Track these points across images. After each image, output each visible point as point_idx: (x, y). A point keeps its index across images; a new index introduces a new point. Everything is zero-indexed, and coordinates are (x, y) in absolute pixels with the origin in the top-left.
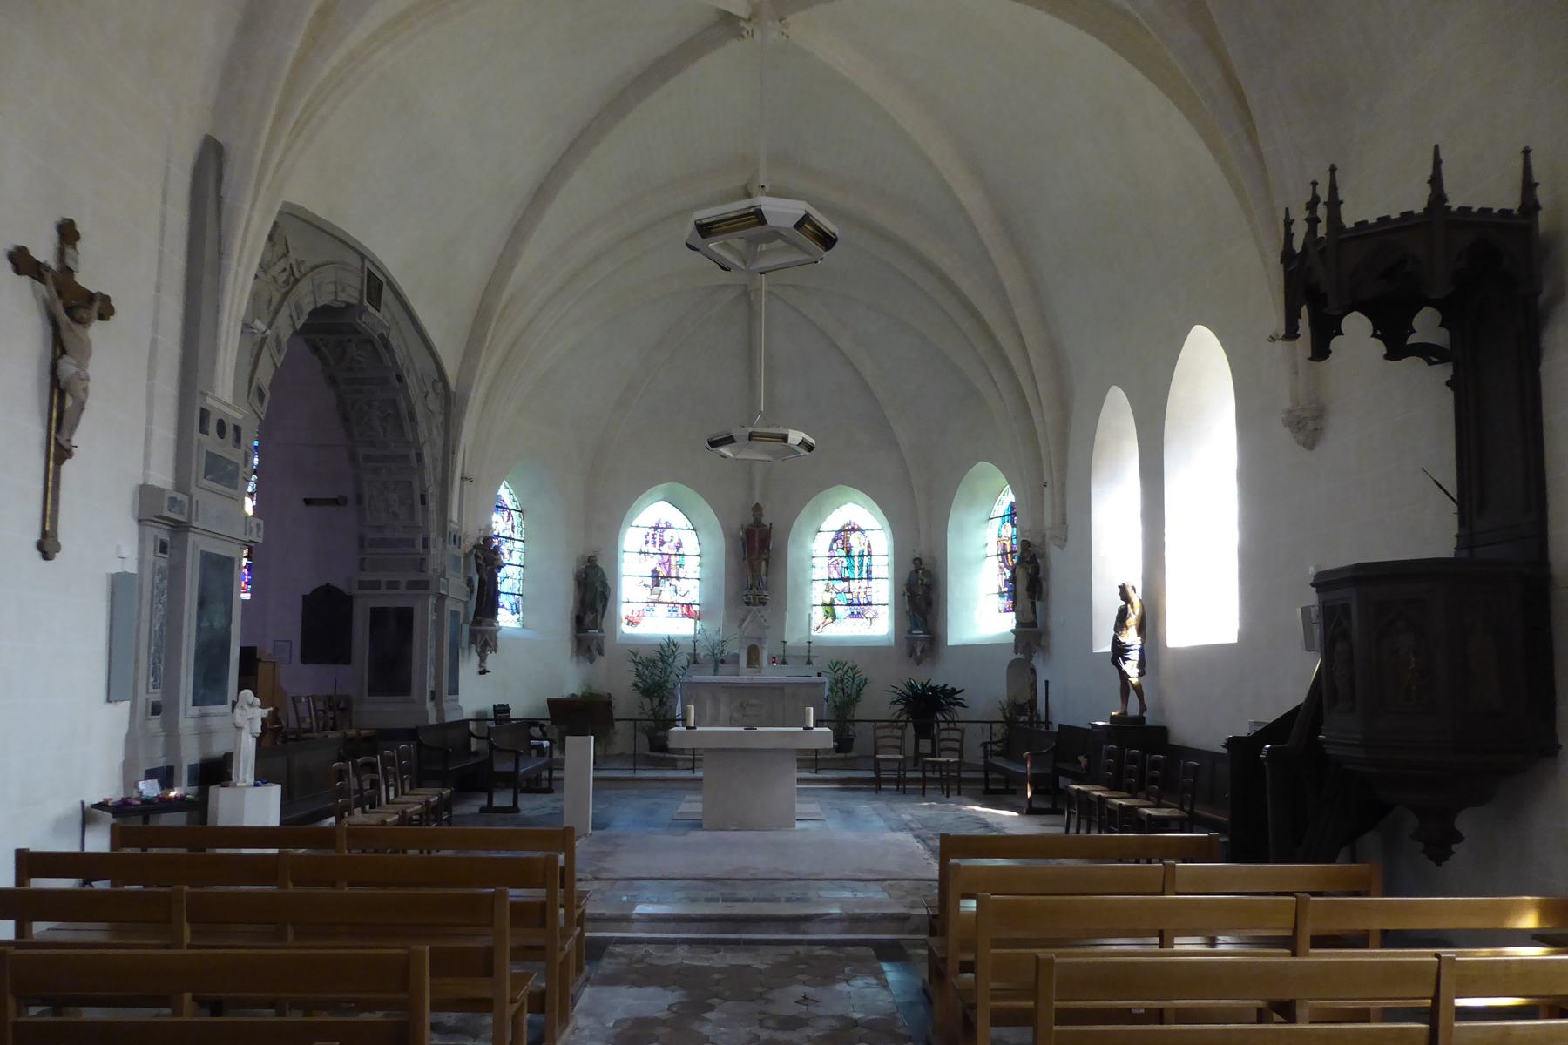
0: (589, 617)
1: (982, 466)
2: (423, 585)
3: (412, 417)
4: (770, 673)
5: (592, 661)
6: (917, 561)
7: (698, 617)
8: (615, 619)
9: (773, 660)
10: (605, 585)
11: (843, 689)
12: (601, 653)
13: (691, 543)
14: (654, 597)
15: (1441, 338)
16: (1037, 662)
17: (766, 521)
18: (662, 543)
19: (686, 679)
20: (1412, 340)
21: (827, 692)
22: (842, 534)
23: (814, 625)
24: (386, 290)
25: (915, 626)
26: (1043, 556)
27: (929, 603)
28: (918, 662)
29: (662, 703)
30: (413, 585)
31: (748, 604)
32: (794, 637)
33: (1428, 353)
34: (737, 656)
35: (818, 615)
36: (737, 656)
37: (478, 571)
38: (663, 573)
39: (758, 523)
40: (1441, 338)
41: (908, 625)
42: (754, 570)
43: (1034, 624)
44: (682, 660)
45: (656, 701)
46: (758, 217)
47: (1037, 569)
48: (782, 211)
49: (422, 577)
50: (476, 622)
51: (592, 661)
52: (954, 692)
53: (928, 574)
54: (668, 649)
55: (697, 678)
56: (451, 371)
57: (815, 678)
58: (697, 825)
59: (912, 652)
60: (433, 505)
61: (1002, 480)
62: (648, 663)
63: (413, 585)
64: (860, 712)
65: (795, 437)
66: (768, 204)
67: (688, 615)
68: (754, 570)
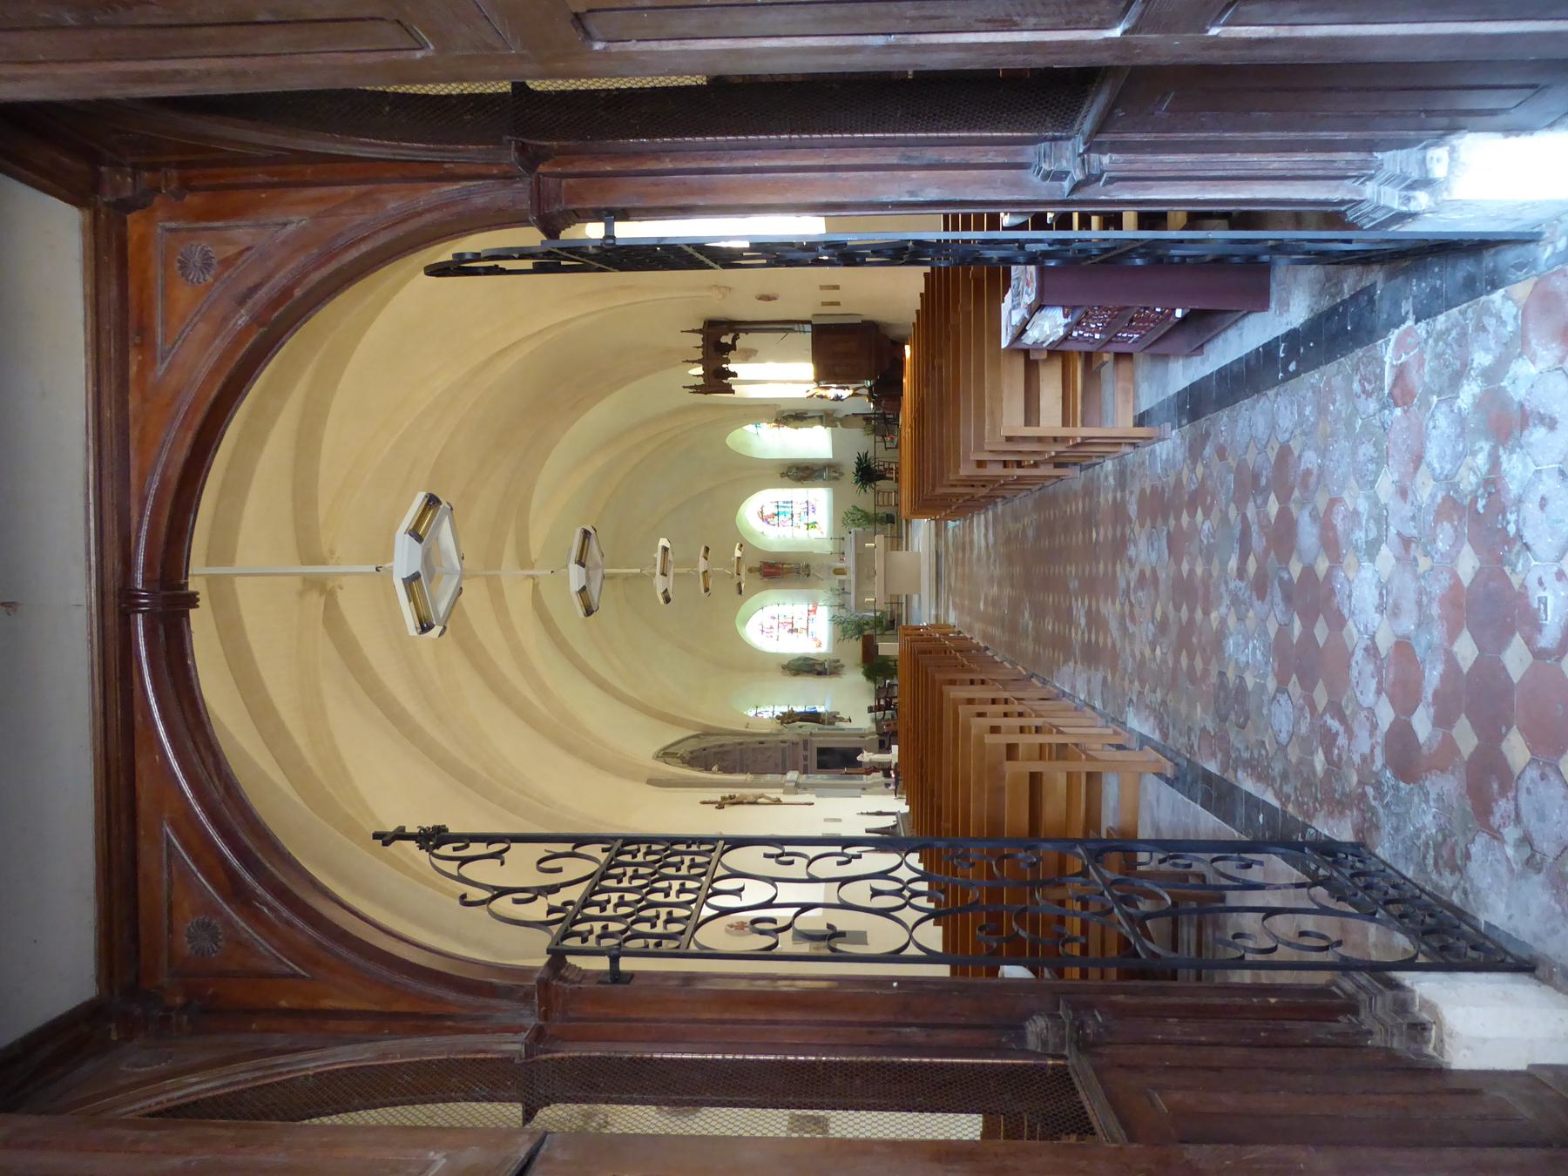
0: (819, 668)
1: (728, 441)
2: (806, 743)
3: (721, 746)
4: (850, 563)
5: (843, 666)
6: (782, 475)
7: (816, 605)
8: (819, 654)
9: (842, 560)
10: (799, 659)
11: (745, 1087)
12: (838, 661)
13: (772, 610)
14: (805, 631)
15: (731, 335)
16: (841, 415)
17: (757, 565)
18: (772, 628)
19: (853, 610)
20: (730, 343)
21: (860, 529)
22: (765, 519)
23: (821, 536)
24: (669, 751)
25: (821, 476)
26: (783, 412)
27: (807, 468)
28: (842, 474)
29: (867, 624)
30: (805, 749)
31: (808, 575)
32: (828, 547)
33: (734, 339)
34: (840, 581)
35: (814, 533)
36: (840, 581)
37: (793, 722)
38: (790, 626)
39: (759, 570)
40: (731, 335)
41: (820, 481)
42: (790, 571)
43: (821, 417)
44: (843, 612)
45: (866, 627)
46: (412, 581)
47: (791, 416)
48: (405, 558)
49: (801, 744)
50: (823, 722)
51: (843, 666)
52: (859, 459)
53: (790, 468)
54: (836, 621)
55: (853, 603)
56: (692, 733)
57: (853, 535)
58: (920, 596)
59: (836, 478)
60: (762, 739)
61: (738, 432)
62: (844, 631)
63: (805, 749)
64: (870, 509)
65: (738, 553)
66: (701, 570)
67: (814, 611)
68: (790, 571)
